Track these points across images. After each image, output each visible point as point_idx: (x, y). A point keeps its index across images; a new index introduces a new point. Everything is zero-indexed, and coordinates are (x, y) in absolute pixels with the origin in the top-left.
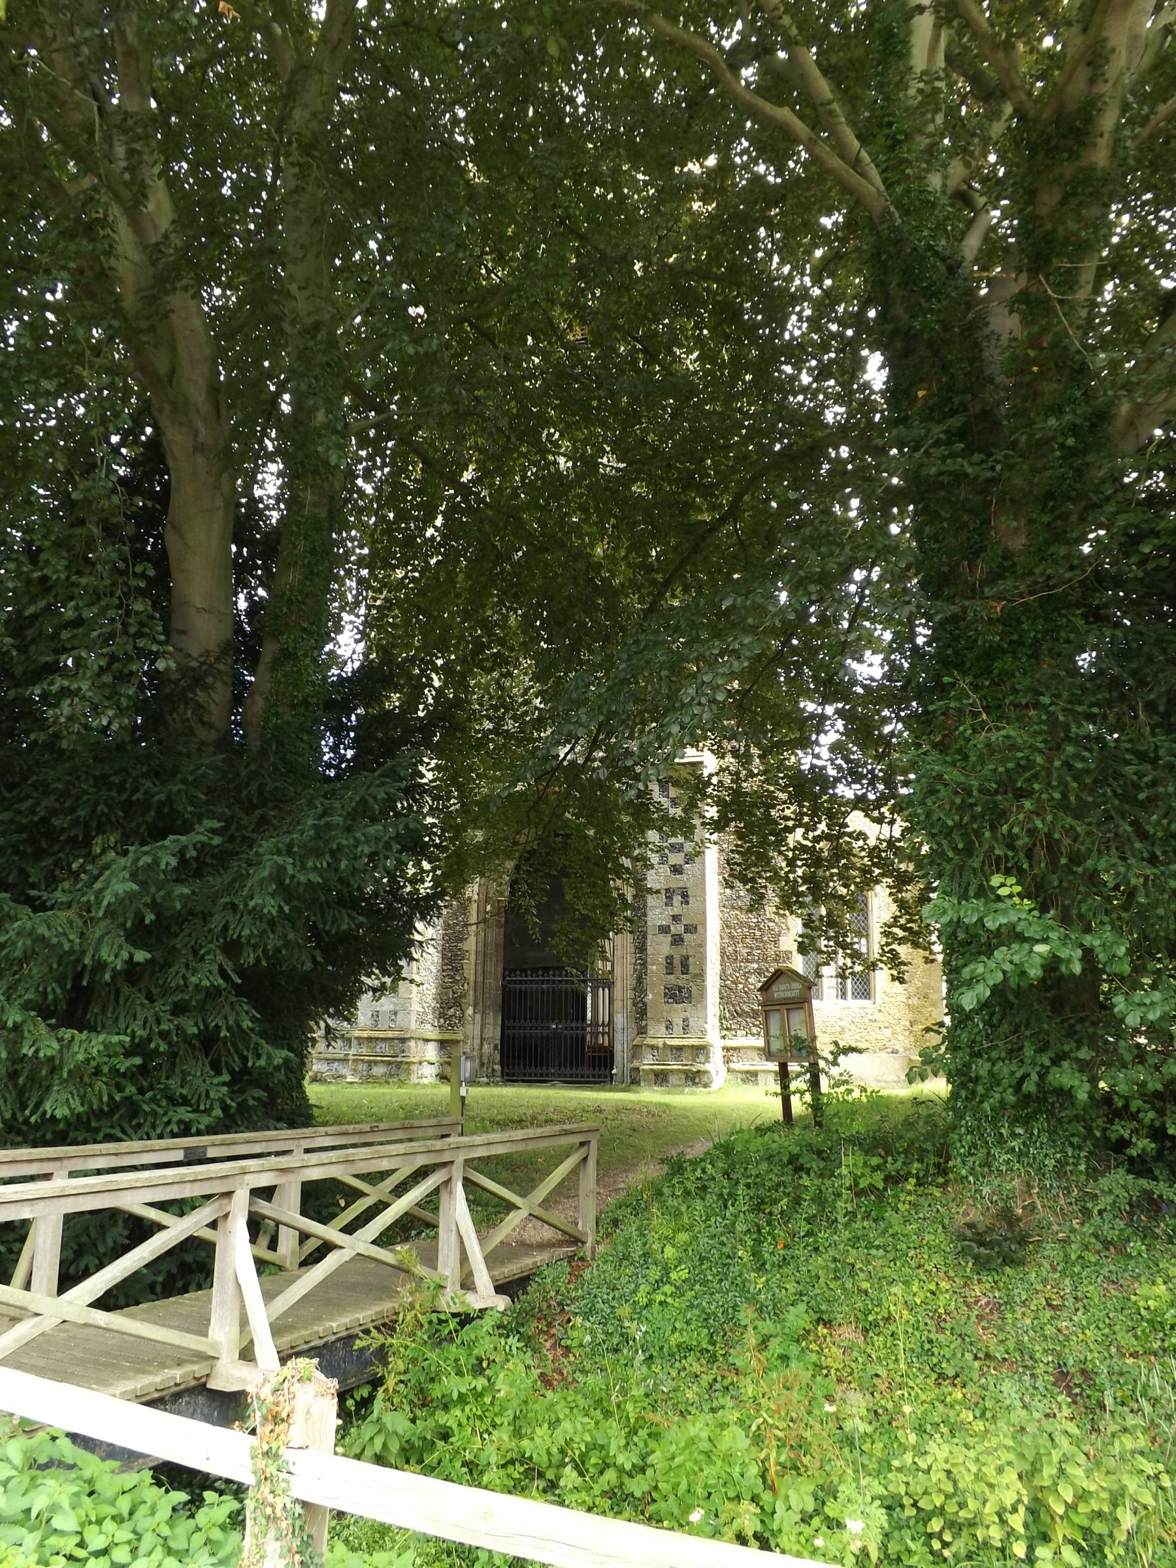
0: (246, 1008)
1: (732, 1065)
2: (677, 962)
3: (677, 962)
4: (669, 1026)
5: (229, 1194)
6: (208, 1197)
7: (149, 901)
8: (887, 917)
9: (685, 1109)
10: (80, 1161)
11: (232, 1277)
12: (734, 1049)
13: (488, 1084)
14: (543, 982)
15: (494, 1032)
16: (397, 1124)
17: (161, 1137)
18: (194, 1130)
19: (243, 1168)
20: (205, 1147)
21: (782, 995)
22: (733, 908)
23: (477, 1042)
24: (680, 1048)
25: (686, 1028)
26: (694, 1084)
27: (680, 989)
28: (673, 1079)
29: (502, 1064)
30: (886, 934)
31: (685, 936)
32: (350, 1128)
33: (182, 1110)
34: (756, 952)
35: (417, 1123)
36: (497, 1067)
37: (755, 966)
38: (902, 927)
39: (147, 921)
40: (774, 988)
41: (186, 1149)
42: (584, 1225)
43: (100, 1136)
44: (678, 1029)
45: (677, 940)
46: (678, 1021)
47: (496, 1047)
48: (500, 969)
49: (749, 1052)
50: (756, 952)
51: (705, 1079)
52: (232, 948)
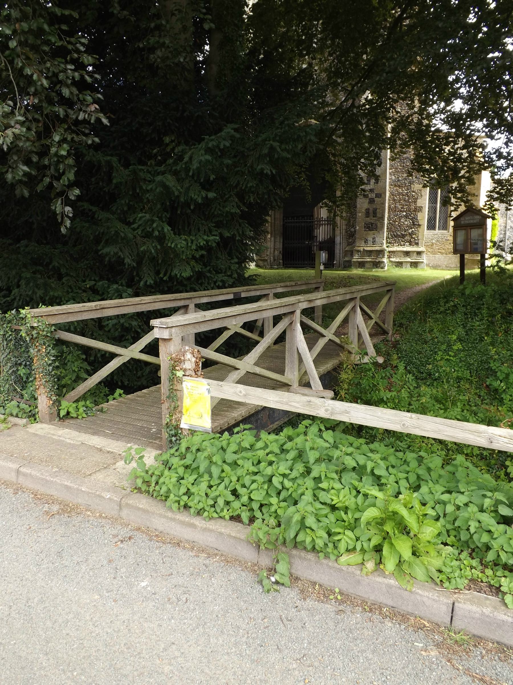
0: (247, 225)
1: (391, 259)
2: (371, 211)
3: (371, 211)
4: (366, 241)
5: (293, 313)
6: (285, 314)
7: (211, 167)
8: (490, 188)
9: (386, 277)
10: (198, 299)
11: (296, 350)
12: (393, 252)
13: (277, 269)
14: (302, 222)
15: (279, 245)
16: (303, 283)
17: (212, 289)
18: (227, 285)
19: (299, 299)
20: (240, 292)
21: (467, 222)
22: (395, 186)
23: (272, 250)
24: (371, 251)
25: (374, 242)
26: (377, 267)
27: (372, 224)
28: (367, 265)
29: (283, 260)
30: (488, 196)
31: (376, 199)
32: (288, 284)
33: (220, 275)
34: (405, 207)
35: (310, 282)
36: (281, 261)
37: (405, 213)
38: (497, 193)
39: (211, 179)
40: (462, 219)
41: (234, 294)
42: (388, 326)
43: (188, 289)
44: (370, 243)
45: (372, 201)
46: (370, 239)
47: (280, 252)
48: (282, 217)
49: (399, 253)
50: (405, 207)
51: (382, 265)
52: (241, 196)
